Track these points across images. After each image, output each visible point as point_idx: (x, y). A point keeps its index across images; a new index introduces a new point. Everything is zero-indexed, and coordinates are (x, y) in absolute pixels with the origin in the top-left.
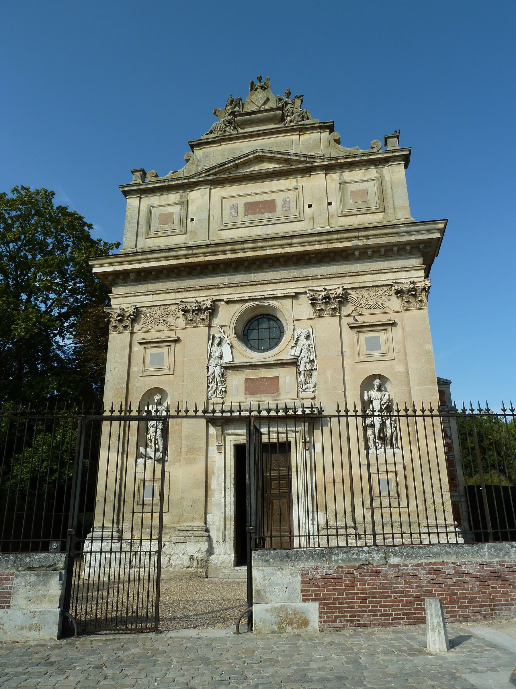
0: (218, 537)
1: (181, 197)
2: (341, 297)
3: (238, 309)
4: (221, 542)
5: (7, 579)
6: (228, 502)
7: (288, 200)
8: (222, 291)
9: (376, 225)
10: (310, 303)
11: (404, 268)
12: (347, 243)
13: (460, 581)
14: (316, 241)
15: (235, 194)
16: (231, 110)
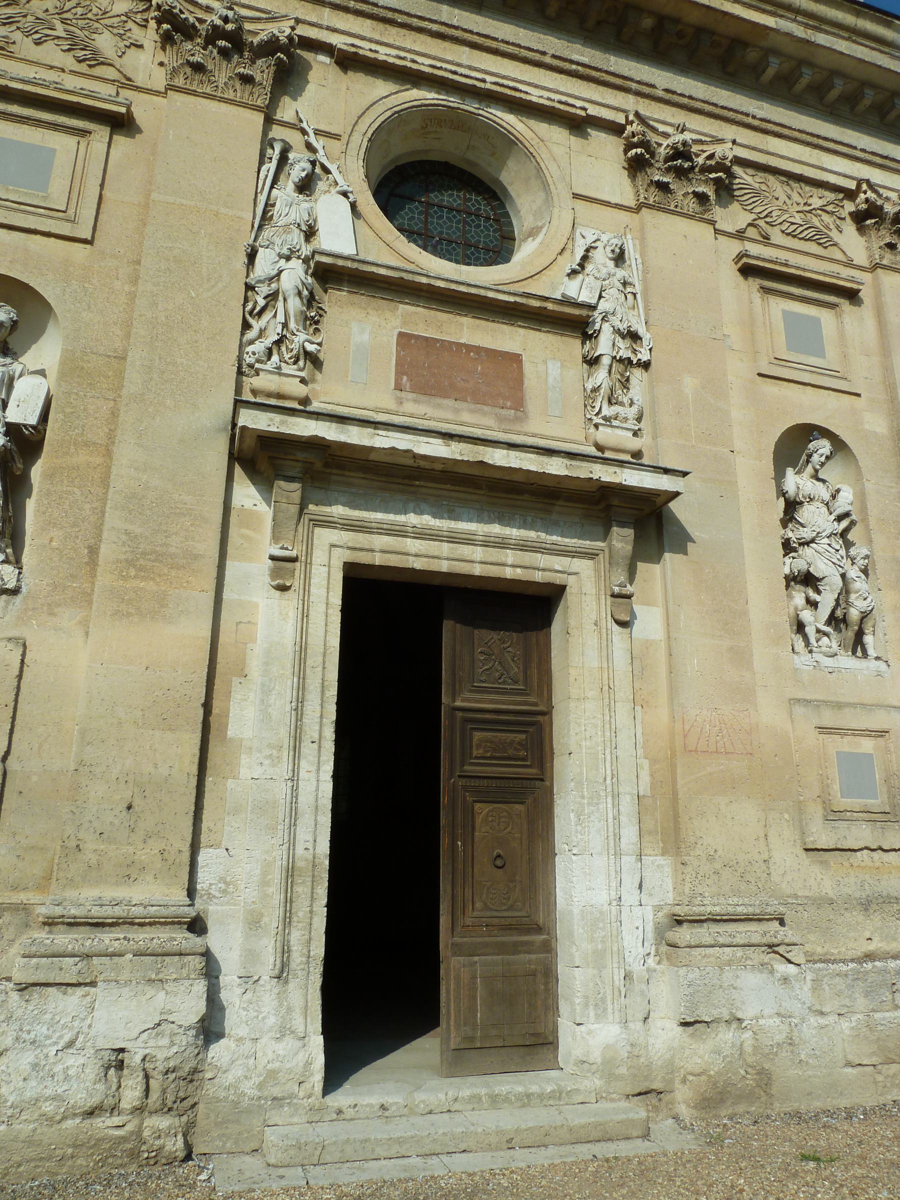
0: (251, 956)
4: (265, 978)
6: (305, 799)
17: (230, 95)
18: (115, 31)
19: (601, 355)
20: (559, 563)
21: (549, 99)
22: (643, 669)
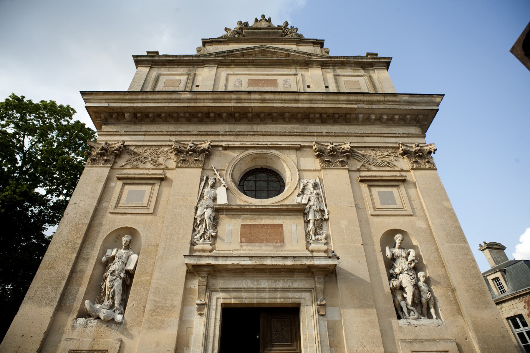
2: (349, 152)
8: (221, 138)
10: (316, 156)
11: (407, 134)
14: (323, 100)
17: (193, 165)
18: (164, 156)
19: (310, 220)
20: (297, 295)
21: (288, 145)
22: (334, 332)
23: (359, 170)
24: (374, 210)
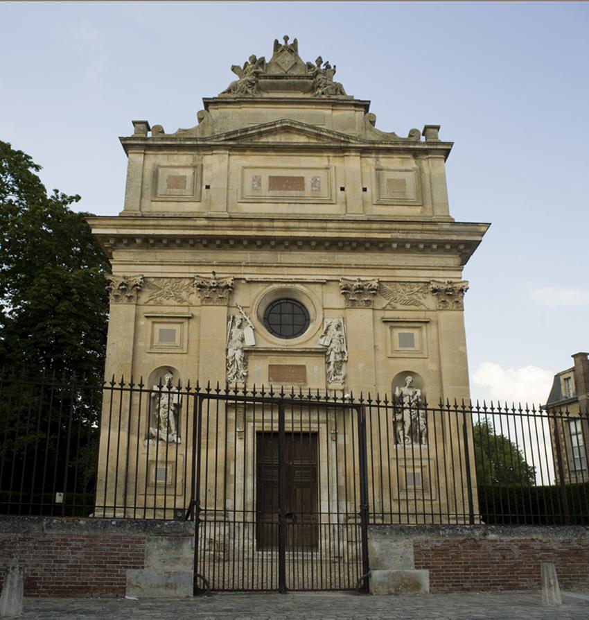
1: (194, 160)
2: (376, 290)
3: (261, 290)
5: (139, 542)
7: (318, 179)
8: (243, 270)
9: (412, 219)
12: (386, 234)
13: (546, 555)
14: (353, 229)
15: (257, 164)
16: (253, 71)
23: (384, 309)
24: (392, 353)
